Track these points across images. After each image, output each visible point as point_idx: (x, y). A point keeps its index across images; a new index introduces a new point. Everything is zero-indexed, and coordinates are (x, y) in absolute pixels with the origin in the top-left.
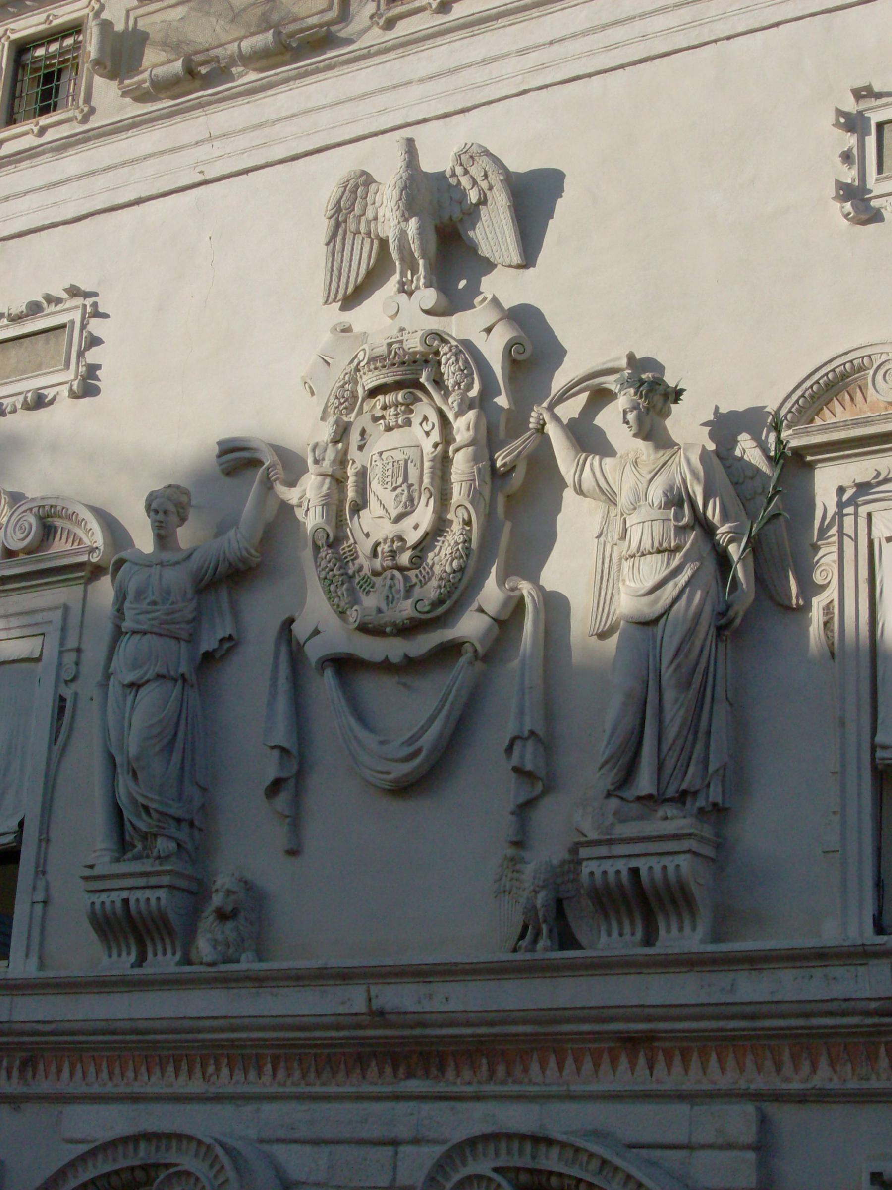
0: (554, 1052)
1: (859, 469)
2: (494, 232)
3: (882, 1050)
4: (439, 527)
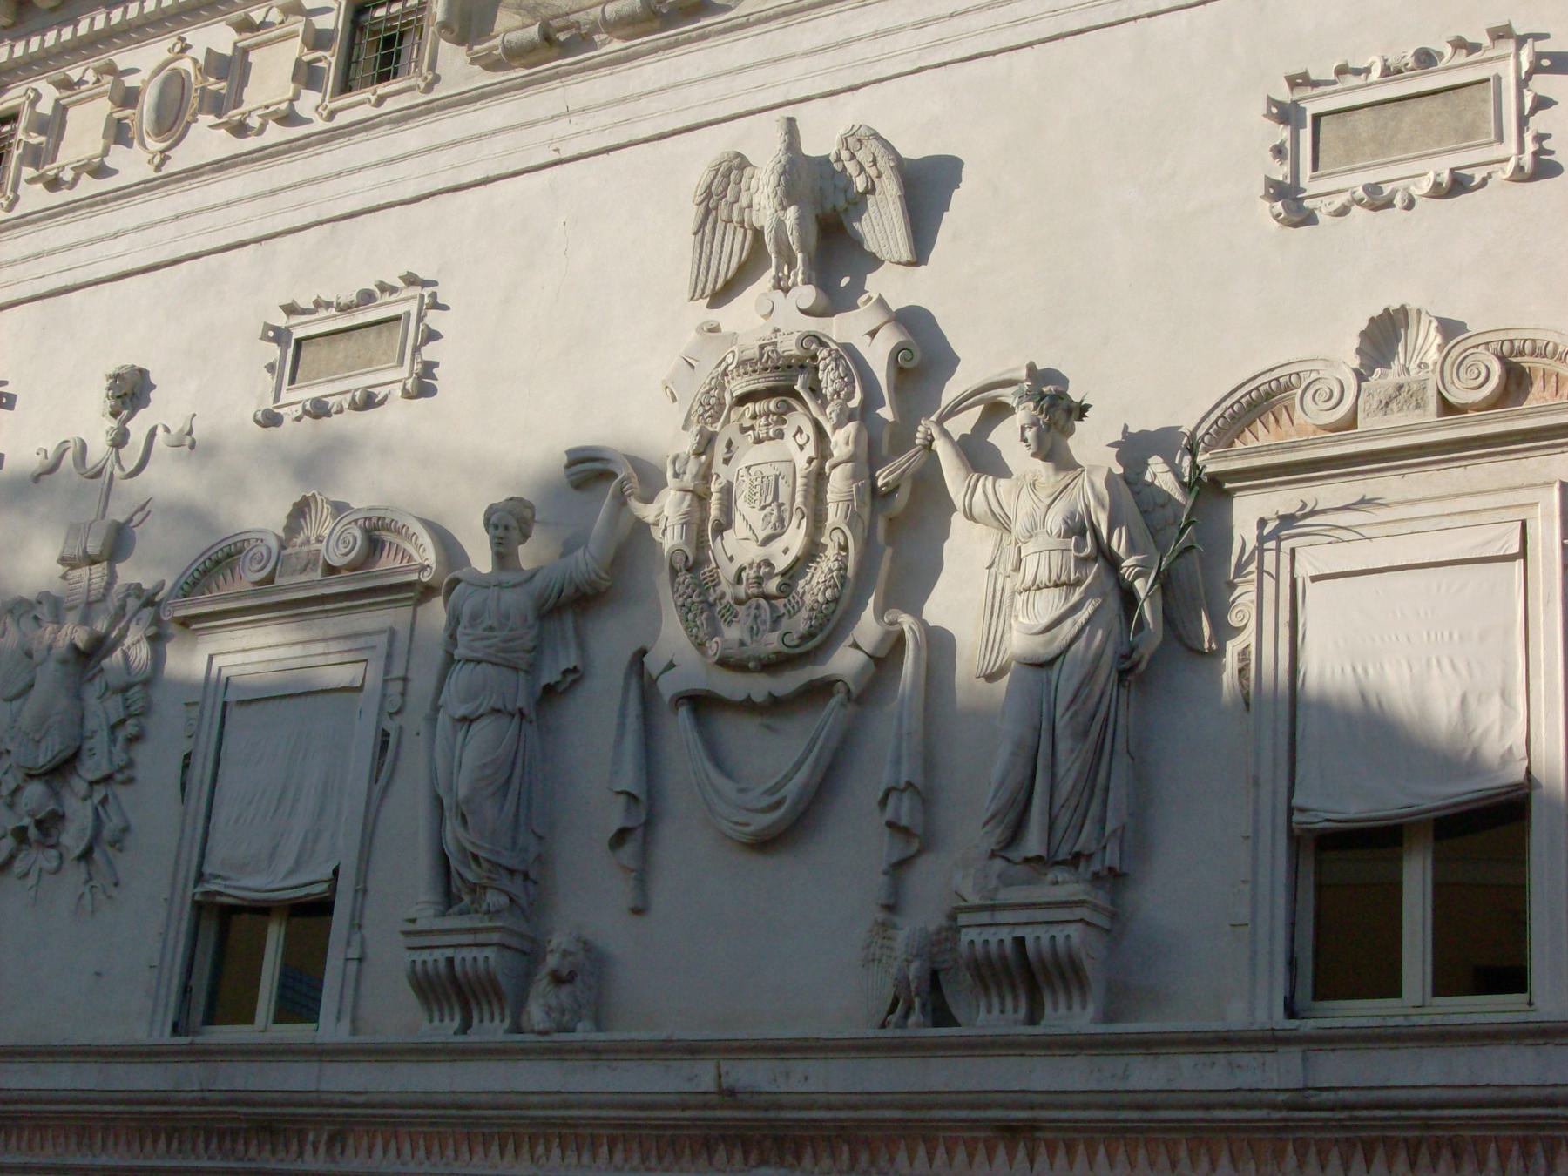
1: (1283, 499)
2: (882, 226)
4: (812, 552)
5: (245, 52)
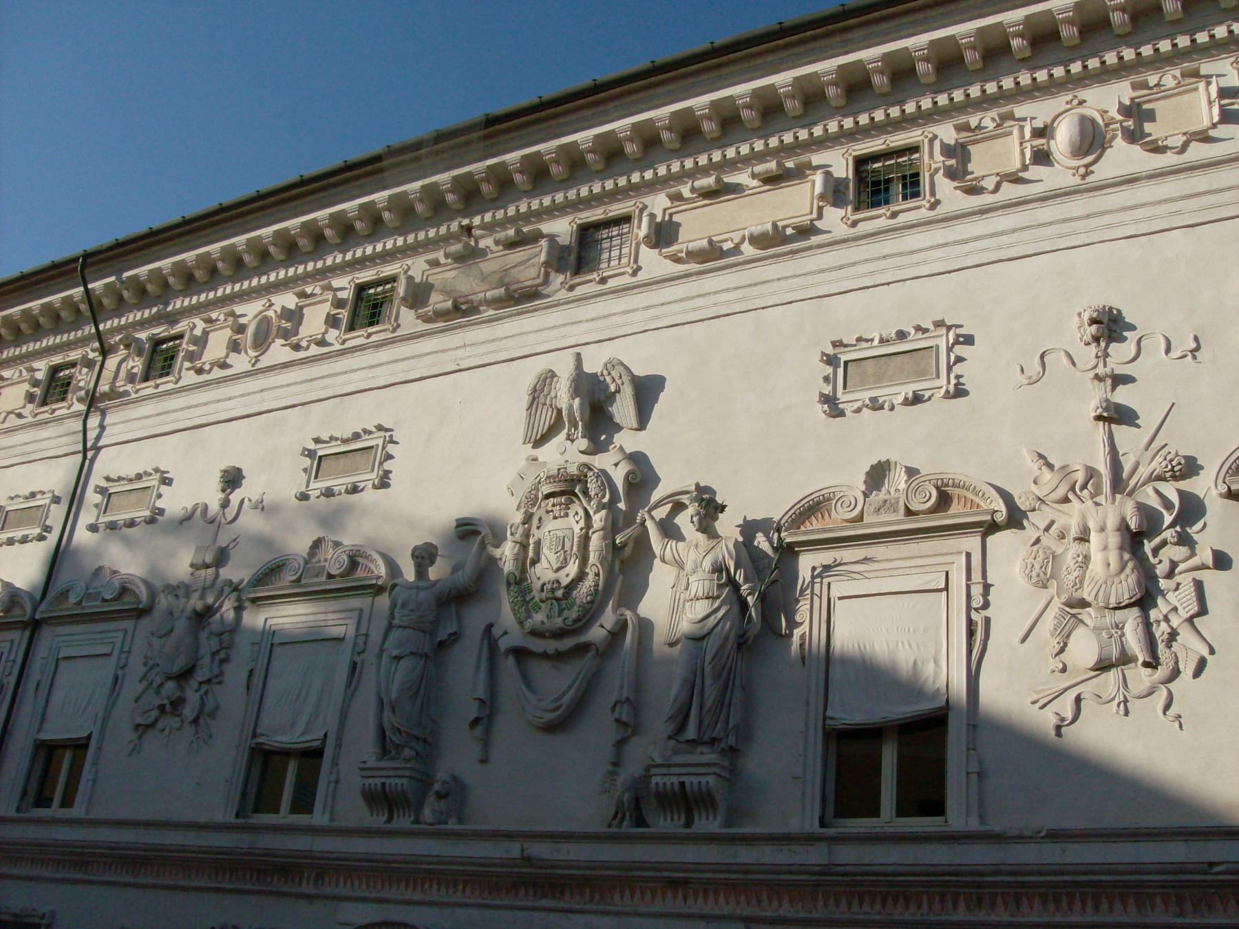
2: (623, 409)
4: (581, 576)
5: (301, 308)
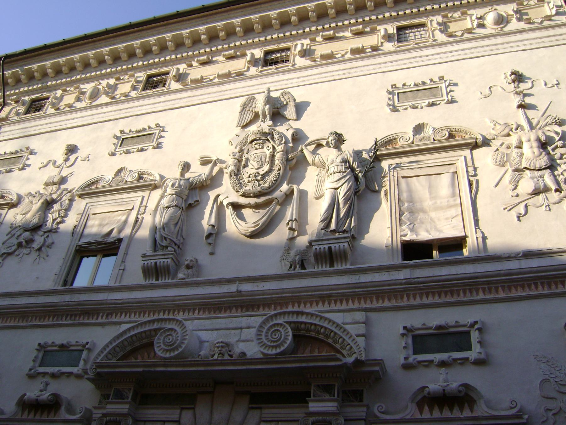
0: (297, 302)
1: (394, 161)
2: (290, 112)
3: (405, 296)
4: (270, 171)
5: (117, 84)
